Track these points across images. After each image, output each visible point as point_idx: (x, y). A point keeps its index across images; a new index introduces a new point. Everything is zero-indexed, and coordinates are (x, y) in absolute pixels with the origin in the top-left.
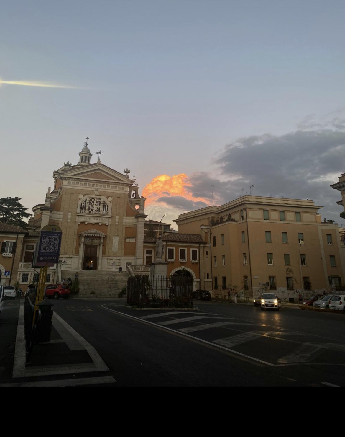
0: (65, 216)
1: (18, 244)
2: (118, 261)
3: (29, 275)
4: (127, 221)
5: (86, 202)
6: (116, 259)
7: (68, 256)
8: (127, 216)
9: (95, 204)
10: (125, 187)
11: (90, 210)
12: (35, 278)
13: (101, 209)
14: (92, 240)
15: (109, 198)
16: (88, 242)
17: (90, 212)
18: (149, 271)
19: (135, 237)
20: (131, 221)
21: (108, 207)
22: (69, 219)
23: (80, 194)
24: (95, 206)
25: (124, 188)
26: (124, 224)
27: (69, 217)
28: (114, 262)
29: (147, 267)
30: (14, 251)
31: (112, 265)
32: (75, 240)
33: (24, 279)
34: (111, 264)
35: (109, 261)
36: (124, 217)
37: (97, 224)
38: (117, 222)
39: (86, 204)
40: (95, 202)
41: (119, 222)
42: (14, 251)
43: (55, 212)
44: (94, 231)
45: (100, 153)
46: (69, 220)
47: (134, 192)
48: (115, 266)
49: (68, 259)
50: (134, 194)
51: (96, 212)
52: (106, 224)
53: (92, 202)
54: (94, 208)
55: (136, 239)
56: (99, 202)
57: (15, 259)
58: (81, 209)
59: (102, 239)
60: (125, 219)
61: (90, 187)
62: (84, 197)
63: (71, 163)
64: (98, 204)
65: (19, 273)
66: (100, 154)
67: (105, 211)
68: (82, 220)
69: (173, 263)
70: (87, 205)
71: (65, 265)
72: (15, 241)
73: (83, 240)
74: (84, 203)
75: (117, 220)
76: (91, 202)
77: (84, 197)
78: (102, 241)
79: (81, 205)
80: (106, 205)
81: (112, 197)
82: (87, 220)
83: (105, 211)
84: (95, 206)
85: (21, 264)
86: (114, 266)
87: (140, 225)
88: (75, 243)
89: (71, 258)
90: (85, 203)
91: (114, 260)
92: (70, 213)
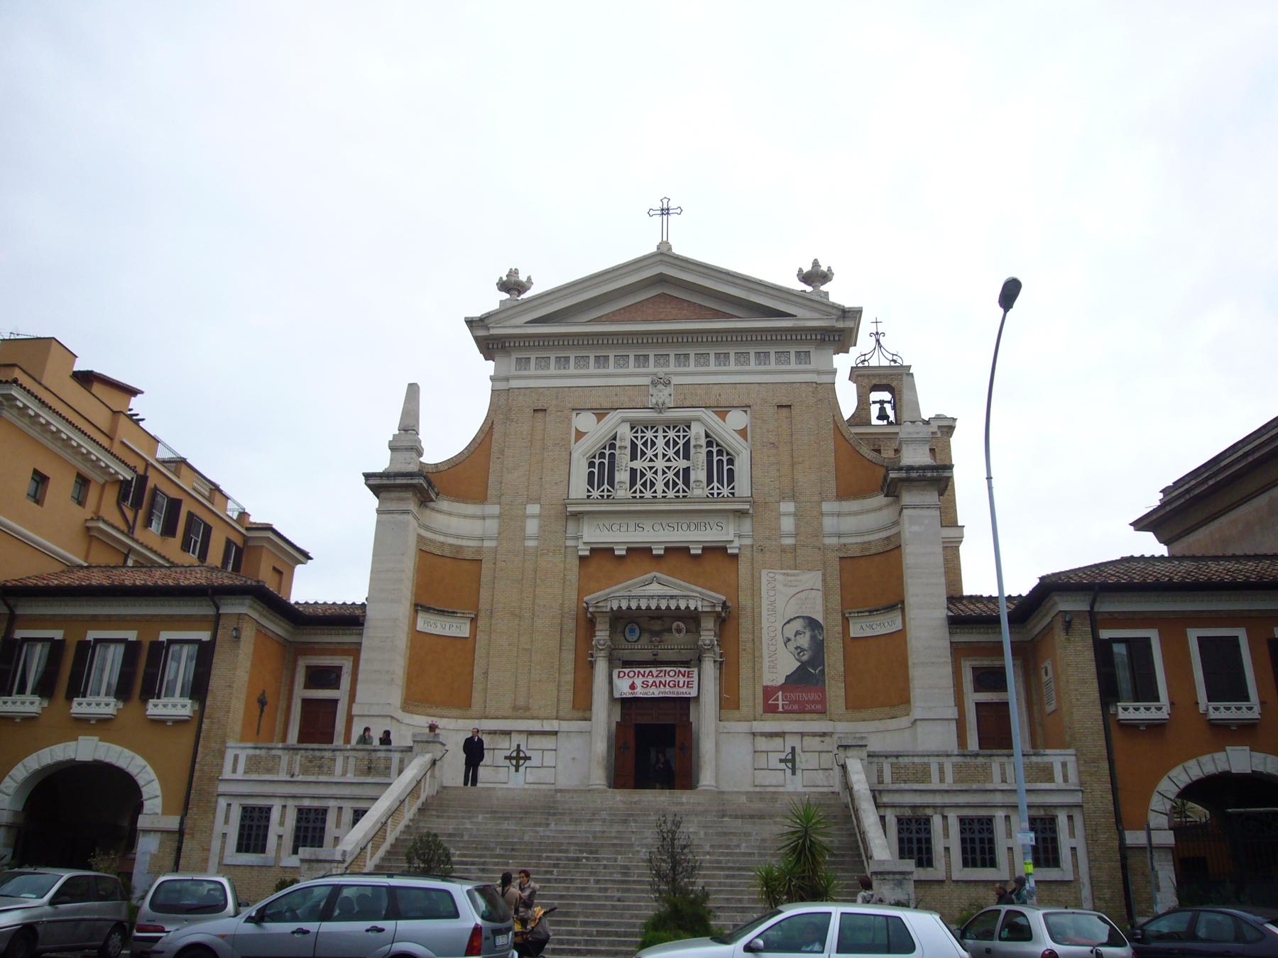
0: (511, 522)
1: (217, 648)
2: (814, 743)
3: (275, 815)
4: (849, 524)
5: (612, 446)
6: (802, 734)
7: (535, 725)
8: (844, 494)
10: (812, 350)
12: (307, 829)
13: (699, 474)
14: (654, 633)
15: (730, 416)
17: (638, 495)
18: (989, 786)
19: (897, 604)
20: (870, 521)
21: (731, 462)
22: (530, 538)
23: (578, 410)
24: (660, 464)
26: (828, 541)
27: (532, 527)
28: (793, 749)
30: (198, 689)
31: (783, 766)
32: (570, 641)
33: (983, 851)
34: (774, 760)
35: (762, 743)
36: (826, 507)
37: (677, 552)
38: (789, 535)
39: (612, 456)
40: (660, 442)
41: (796, 535)
42: (198, 689)
43: (444, 504)
44: (653, 590)
45: (665, 212)
46: (531, 543)
47: (886, 396)
48: (799, 772)
49: (537, 738)
50: (888, 407)
51: (671, 494)
52: (725, 549)
54: (660, 456)
55: (903, 610)
57: (204, 726)
58: (591, 483)
59: (708, 624)
60: (832, 514)
61: (625, 375)
62: (599, 421)
63: (529, 278)
64: (643, 475)
65: (222, 803)
67: (715, 484)
68: (594, 534)
69: (1155, 728)
70: (623, 458)
72: (205, 636)
73: (602, 634)
74: (602, 455)
75: (787, 524)
77: (599, 421)
78: (707, 635)
79: (591, 464)
81: (745, 407)
82: (620, 536)
83: (715, 484)
84: (660, 464)
85: (236, 757)
86: (794, 773)
87: (916, 528)
88: (569, 657)
89: (556, 733)
90: (607, 452)
91: (792, 741)
92: (533, 509)
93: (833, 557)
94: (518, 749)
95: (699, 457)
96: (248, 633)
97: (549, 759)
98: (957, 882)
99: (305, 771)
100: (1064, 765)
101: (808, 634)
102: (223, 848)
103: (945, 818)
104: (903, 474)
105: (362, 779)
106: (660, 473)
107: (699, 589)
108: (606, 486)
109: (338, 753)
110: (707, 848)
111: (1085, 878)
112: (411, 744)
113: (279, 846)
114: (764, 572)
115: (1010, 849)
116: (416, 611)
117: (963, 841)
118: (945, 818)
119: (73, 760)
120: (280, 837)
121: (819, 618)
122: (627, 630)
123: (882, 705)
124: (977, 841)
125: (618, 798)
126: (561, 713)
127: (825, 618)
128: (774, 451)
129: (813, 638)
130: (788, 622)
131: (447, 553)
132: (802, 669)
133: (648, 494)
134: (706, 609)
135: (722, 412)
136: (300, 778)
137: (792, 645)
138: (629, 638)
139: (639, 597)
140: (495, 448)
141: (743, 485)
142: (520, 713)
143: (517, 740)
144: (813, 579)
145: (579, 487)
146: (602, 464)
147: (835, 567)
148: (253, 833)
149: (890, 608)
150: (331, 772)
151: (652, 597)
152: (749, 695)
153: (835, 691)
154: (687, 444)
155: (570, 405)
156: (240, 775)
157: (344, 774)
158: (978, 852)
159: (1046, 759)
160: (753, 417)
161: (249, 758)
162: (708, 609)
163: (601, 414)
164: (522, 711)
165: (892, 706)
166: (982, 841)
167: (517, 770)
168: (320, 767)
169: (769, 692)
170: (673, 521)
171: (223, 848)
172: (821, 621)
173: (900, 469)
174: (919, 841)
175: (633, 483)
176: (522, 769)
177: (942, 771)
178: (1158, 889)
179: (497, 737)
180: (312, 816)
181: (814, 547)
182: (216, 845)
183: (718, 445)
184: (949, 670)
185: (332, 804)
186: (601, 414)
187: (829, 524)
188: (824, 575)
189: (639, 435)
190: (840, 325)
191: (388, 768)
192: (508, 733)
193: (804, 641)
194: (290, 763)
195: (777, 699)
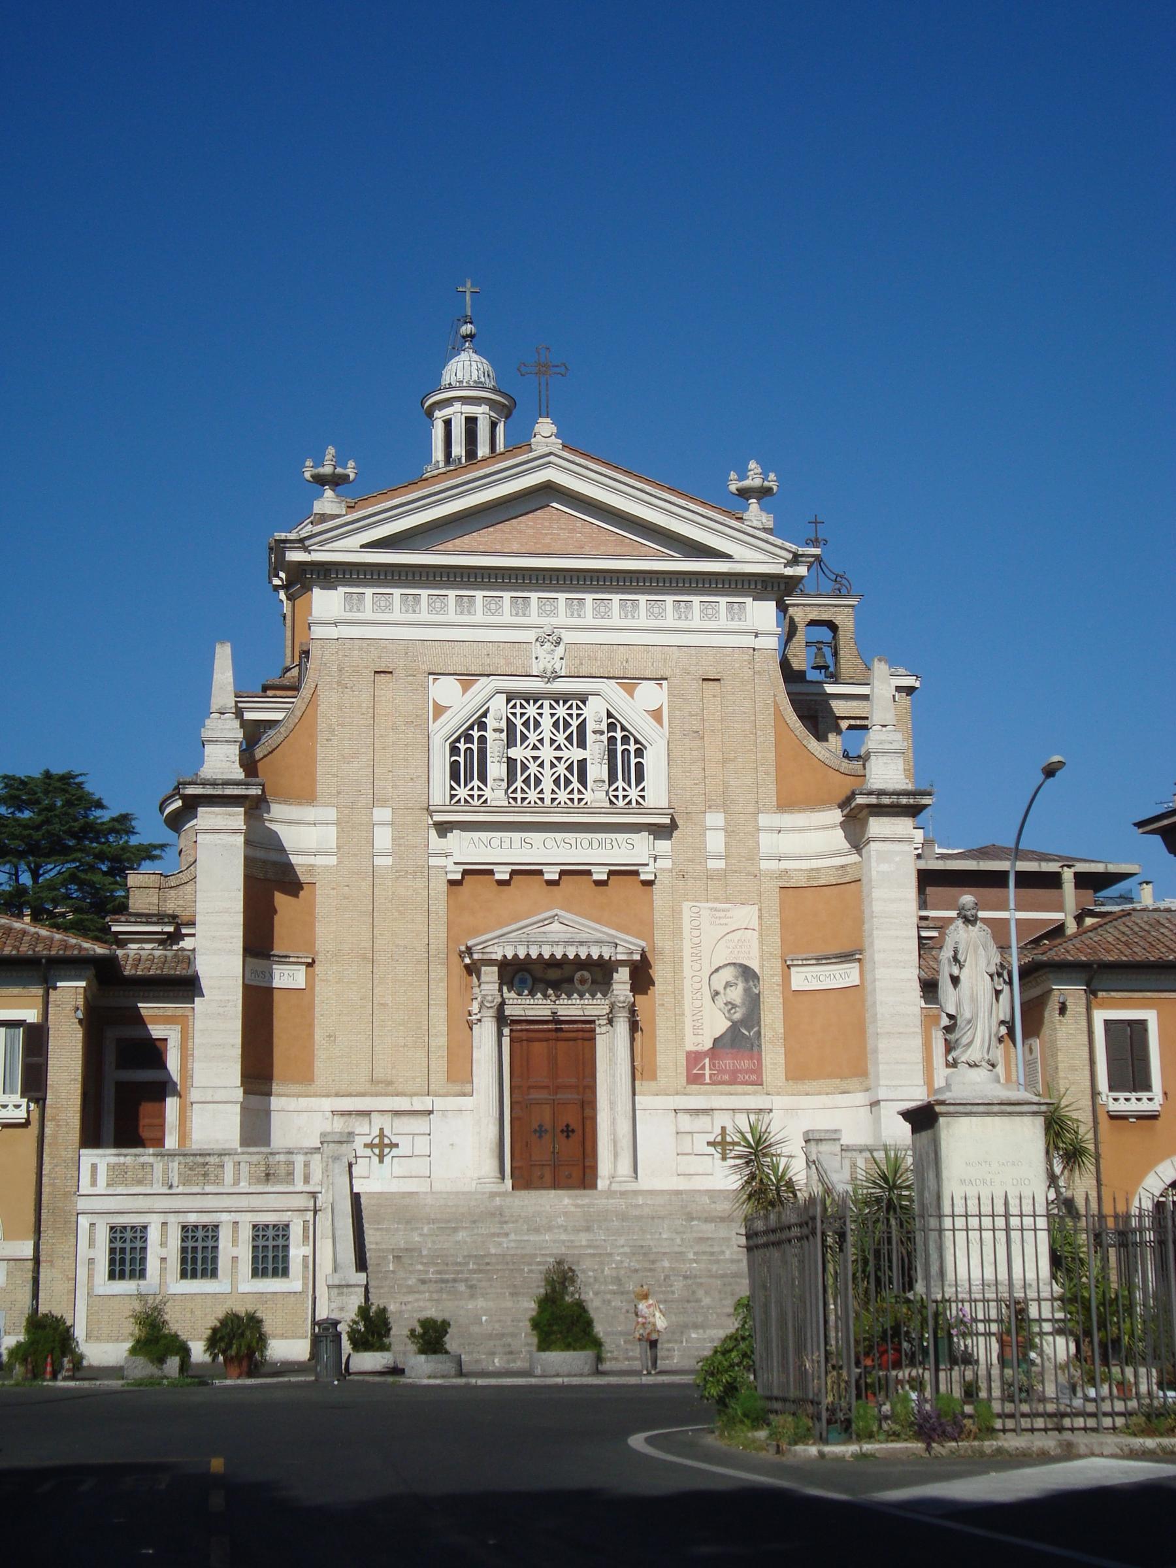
3: (153, 1235)
5: (482, 726)
7: (402, 1103)
12: (195, 1249)
13: (597, 771)
21: (639, 753)
22: (381, 854)
26: (765, 865)
27: (383, 838)
31: (711, 1150)
35: (685, 1122)
36: (764, 820)
39: (482, 739)
40: (547, 723)
41: (727, 857)
44: (561, 933)
49: (405, 1119)
58: (454, 776)
59: (622, 975)
65: (84, 1222)
67: (620, 783)
68: (468, 849)
74: (469, 739)
77: (465, 691)
79: (454, 750)
80: (625, 740)
82: (503, 851)
83: (620, 783)
85: (94, 1167)
87: (884, 867)
88: (439, 1014)
90: (476, 734)
92: (382, 814)
93: (771, 888)
94: (382, 1134)
97: (421, 1145)
99: (186, 1181)
101: (741, 986)
102: (91, 1277)
104: (873, 800)
105: (260, 1188)
106: (547, 765)
109: (226, 1158)
110: (691, 1256)
113: (163, 1270)
114: (686, 906)
117: (112, 1251)
120: (163, 1259)
121: (754, 965)
122: (516, 980)
123: (830, 1076)
125: (566, 1201)
126: (432, 1087)
127: (762, 966)
128: (698, 742)
129: (747, 991)
130: (717, 970)
132: (735, 1027)
133: (532, 795)
134: (620, 957)
135: (629, 682)
136: (180, 1189)
137: (721, 1000)
139: (540, 944)
141: (656, 793)
142: (380, 1088)
143: (378, 1121)
144: (747, 915)
147: (773, 899)
148: (126, 1257)
149: (846, 957)
150: (219, 1181)
151: (557, 943)
152: (669, 1060)
153: (773, 1057)
155: (425, 667)
156: (101, 1187)
157: (237, 1182)
160: (671, 694)
161: (112, 1168)
162: (624, 957)
163: (467, 679)
164: (380, 1085)
165: (842, 1078)
168: (205, 1175)
169: (694, 1058)
170: (570, 836)
171: (91, 1277)
172: (757, 970)
173: (870, 793)
175: (511, 779)
176: (387, 1159)
179: (353, 1119)
180: (128, 1235)
181: (749, 874)
183: (623, 729)
184: (918, 1042)
185: (225, 1217)
186: (467, 679)
187: (767, 842)
188: (760, 910)
190: (789, 571)
191: (291, 1174)
192: (367, 1114)
193: (736, 994)
194: (166, 1172)
195: (703, 1068)
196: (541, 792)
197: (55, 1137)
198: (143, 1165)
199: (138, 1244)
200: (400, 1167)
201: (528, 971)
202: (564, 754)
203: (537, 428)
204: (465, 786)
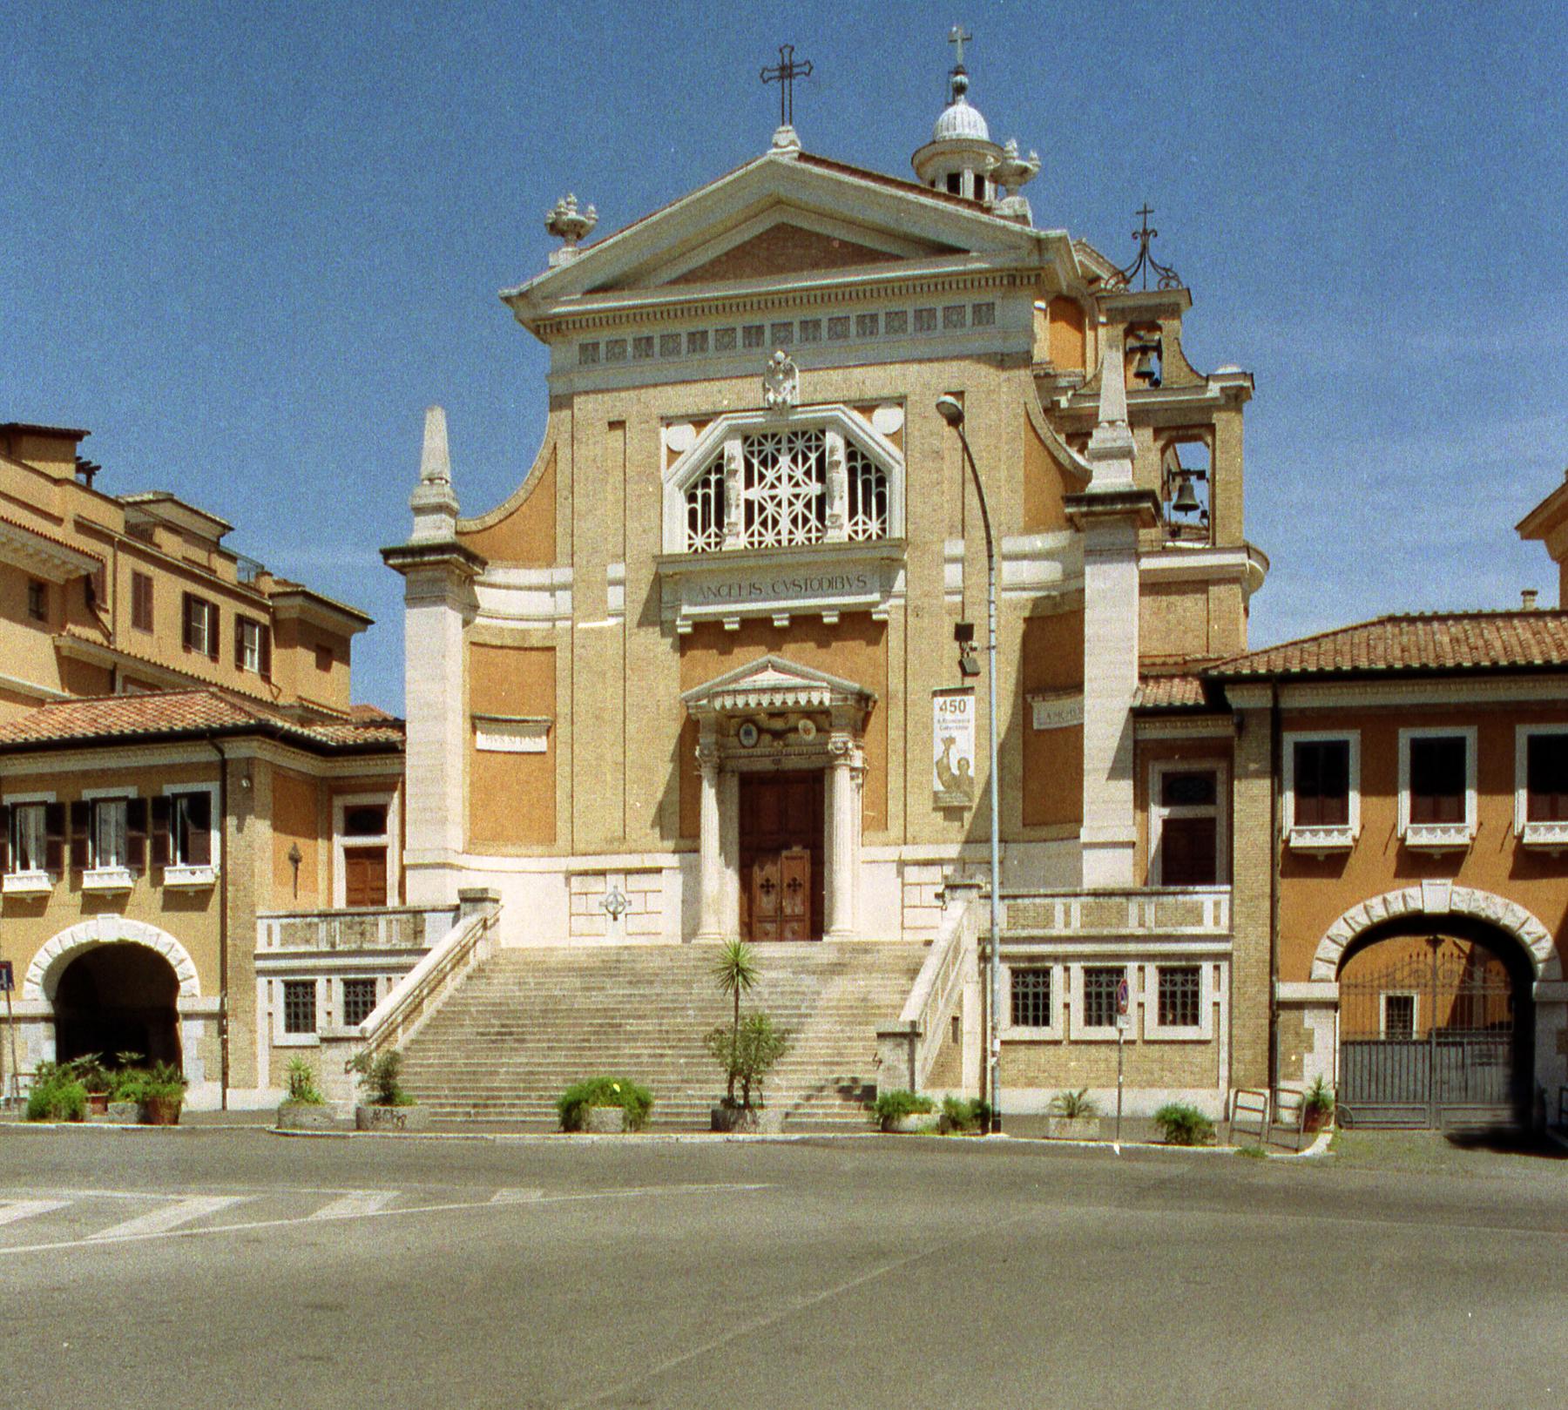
5: (719, 469)
9: (785, 509)
11: (757, 520)
13: (840, 506)
16: (758, 751)
18: (1124, 931)
21: (881, 482)
25: (991, 306)
29: (1118, 900)
33: (1026, 1008)
40: (785, 524)
52: (868, 614)
53: (806, 520)
54: (785, 479)
56: (756, 526)
58: (693, 525)
64: (762, 509)
66: (791, 67)
67: (860, 517)
71: (620, 917)
74: (706, 484)
76: (814, 522)
79: (692, 498)
81: (900, 402)
83: (860, 517)
90: (713, 478)
95: (840, 477)
96: (262, 780)
98: (1076, 1042)
100: (1217, 904)
103: (1067, 969)
106: (785, 504)
107: (827, 676)
108: (713, 529)
111: (1224, 1038)
112: (458, 902)
115: (1141, 1005)
116: (474, 729)
117: (1088, 995)
118: (1067, 969)
119: (96, 942)
124: (1179, 994)
131: (509, 642)
138: (745, 742)
140: (562, 480)
145: (677, 538)
146: (706, 498)
154: (821, 460)
155: (656, 412)
158: (1104, 1006)
159: (1195, 897)
166: (305, 1004)
167: (615, 919)
174: (1036, 995)
175: (749, 521)
177: (1067, 912)
178: (1310, 1049)
179: (590, 879)
182: (262, 1025)
189: (756, 448)
192: (603, 873)
196: (779, 533)
197: (234, 901)
198: (310, 925)
199: (1189, 988)
200: (635, 924)
201: (754, 723)
202: (767, 493)
203: (777, 138)
204: (704, 531)
